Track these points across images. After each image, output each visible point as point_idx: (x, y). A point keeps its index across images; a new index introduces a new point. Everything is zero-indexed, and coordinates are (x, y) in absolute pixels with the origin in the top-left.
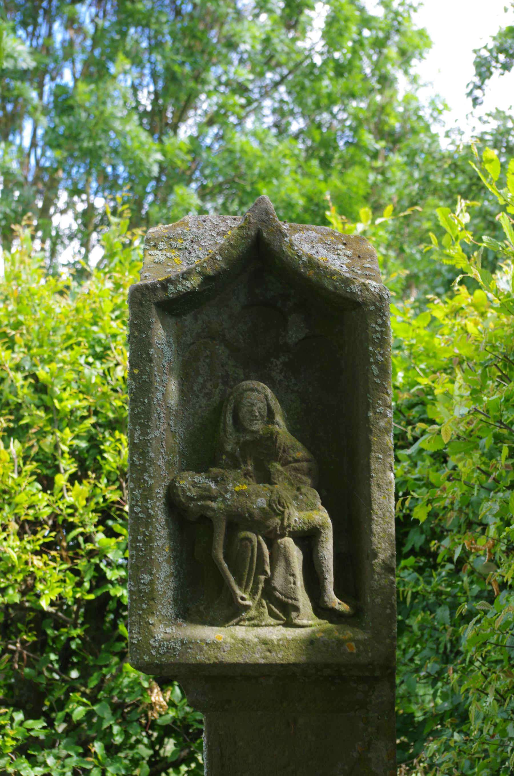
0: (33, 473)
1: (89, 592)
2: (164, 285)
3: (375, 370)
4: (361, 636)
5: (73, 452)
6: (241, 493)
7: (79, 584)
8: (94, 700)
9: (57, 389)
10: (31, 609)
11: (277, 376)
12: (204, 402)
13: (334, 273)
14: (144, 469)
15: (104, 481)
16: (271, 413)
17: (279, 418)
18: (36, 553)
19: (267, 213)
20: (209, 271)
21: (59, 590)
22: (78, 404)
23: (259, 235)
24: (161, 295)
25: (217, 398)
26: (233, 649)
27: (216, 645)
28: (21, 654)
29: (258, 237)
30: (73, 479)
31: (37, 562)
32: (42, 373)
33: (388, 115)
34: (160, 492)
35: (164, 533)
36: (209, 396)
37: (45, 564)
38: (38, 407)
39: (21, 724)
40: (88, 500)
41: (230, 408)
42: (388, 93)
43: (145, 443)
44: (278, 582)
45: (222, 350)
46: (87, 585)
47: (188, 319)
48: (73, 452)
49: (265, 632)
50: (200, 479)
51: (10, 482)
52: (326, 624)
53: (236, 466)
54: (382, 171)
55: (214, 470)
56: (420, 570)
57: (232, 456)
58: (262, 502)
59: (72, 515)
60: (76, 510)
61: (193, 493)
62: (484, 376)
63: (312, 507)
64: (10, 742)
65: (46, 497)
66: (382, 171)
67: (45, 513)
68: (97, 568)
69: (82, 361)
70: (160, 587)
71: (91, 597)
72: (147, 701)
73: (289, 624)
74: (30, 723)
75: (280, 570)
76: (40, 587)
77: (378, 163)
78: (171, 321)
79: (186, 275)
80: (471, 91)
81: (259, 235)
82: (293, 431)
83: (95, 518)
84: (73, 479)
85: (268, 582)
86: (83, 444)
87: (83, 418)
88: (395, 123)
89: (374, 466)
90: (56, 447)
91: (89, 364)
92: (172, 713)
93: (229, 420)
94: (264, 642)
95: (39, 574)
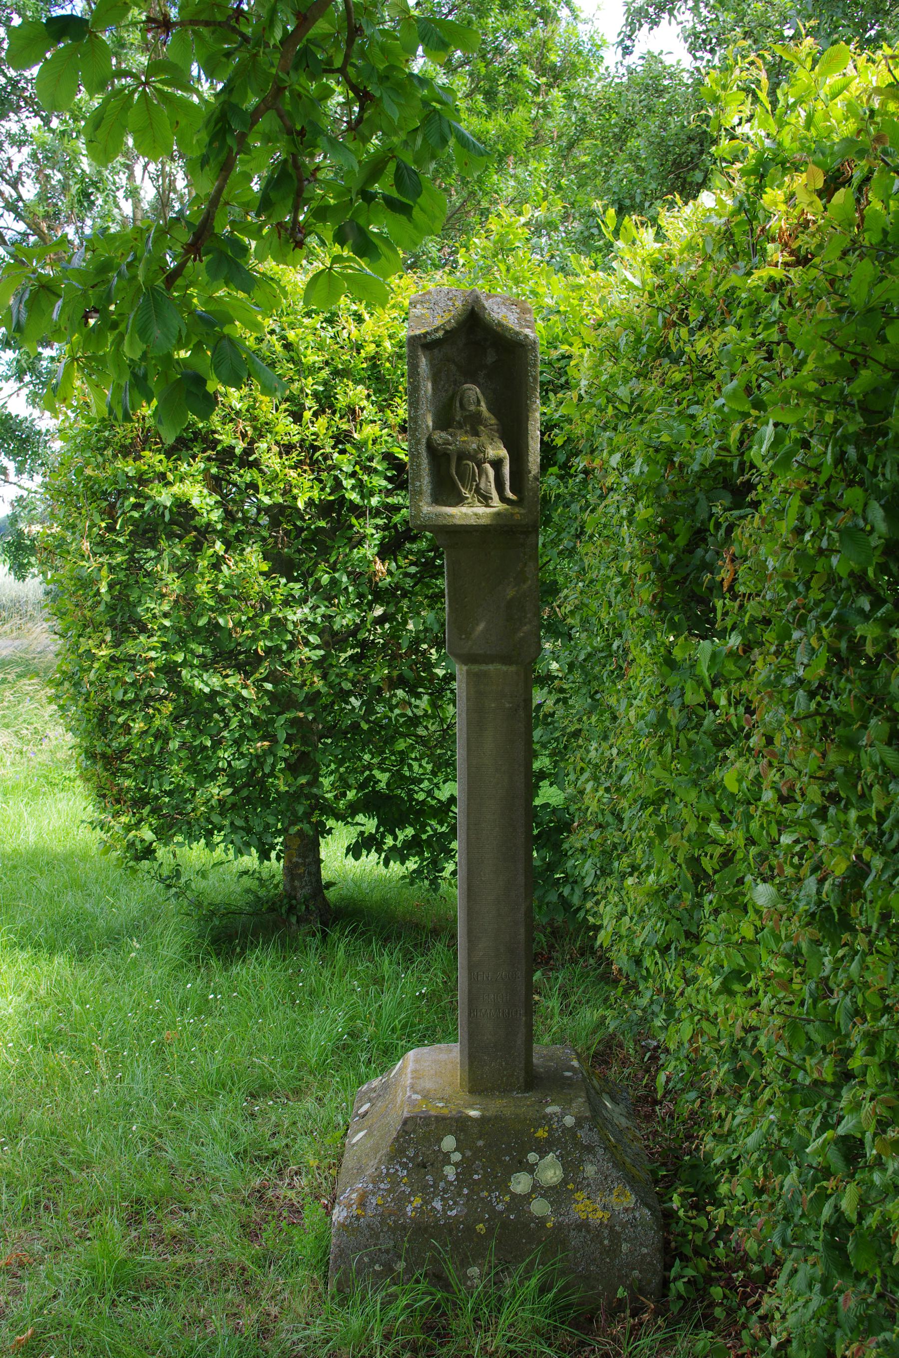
0: (286, 411)
1: (330, 494)
2: (425, 335)
3: (531, 379)
4: (523, 511)
5: (315, 394)
6: (464, 442)
7: (322, 489)
8: (335, 570)
9: (302, 348)
10: (290, 507)
11: (482, 381)
12: (444, 394)
13: (511, 329)
14: (416, 430)
15: (338, 415)
16: (479, 401)
17: (483, 404)
18: (291, 467)
19: (477, 297)
20: (448, 328)
21: (309, 494)
22: (317, 359)
23: (473, 309)
24: (423, 341)
25: (450, 393)
26: (460, 517)
27: (452, 516)
28: (283, 540)
29: (473, 311)
30: (316, 414)
31: (293, 473)
32: (291, 335)
33: (549, 50)
34: (424, 441)
35: (426, 461)
36: (446, 391)
37: (299, 475)
38: (288, 361)
39: (285, 585)
40: (327, 429)
41: (458, 398)
42: (550, 27)
43: (416, 417)
44: (482, 486)
45: (453, 367)
46: (328, 490)
47: (436, 351)
48: (315, 394)
49: (475, 510)
50: (443, 434)
51: (270, 416)
52: (506, 506)
53: (461, 428)
54: (543, 106)
55: (450, 430)
56: (561, 477)
57: (459, 422)
58: (474, 446)
59: (315, 440)
60: (318, 436)
61: (440, 441)
62: (601, 357)
63: (499, 449)
64: (279, 597)
65: (297, 427)
66: (543, 106)
67: (296, 439)
68: (336, 478)
69: (318, 326)
70: (424, 488)
71: (332, 498)
72: (372, 569)
73: (487, 506)
74: (291, 585)
75: (483, 479)
76: (295, 491)
77: (539, 99)
78: (427, 353)
79: (436, 330)
80: (623, 40)
81: (473, 309)
82: (489, 409)
83: (332, 442)
84: (316, 414)
85: (477, 485)
86: (321, 388)
87: (321, 369)
88: (554, 58)
89: (530, 428)
90: (302, 390)
91: (322, 328)
92: (388, 579)
93: (458, 405)
94: (476, 515)
95: (294, 482)
